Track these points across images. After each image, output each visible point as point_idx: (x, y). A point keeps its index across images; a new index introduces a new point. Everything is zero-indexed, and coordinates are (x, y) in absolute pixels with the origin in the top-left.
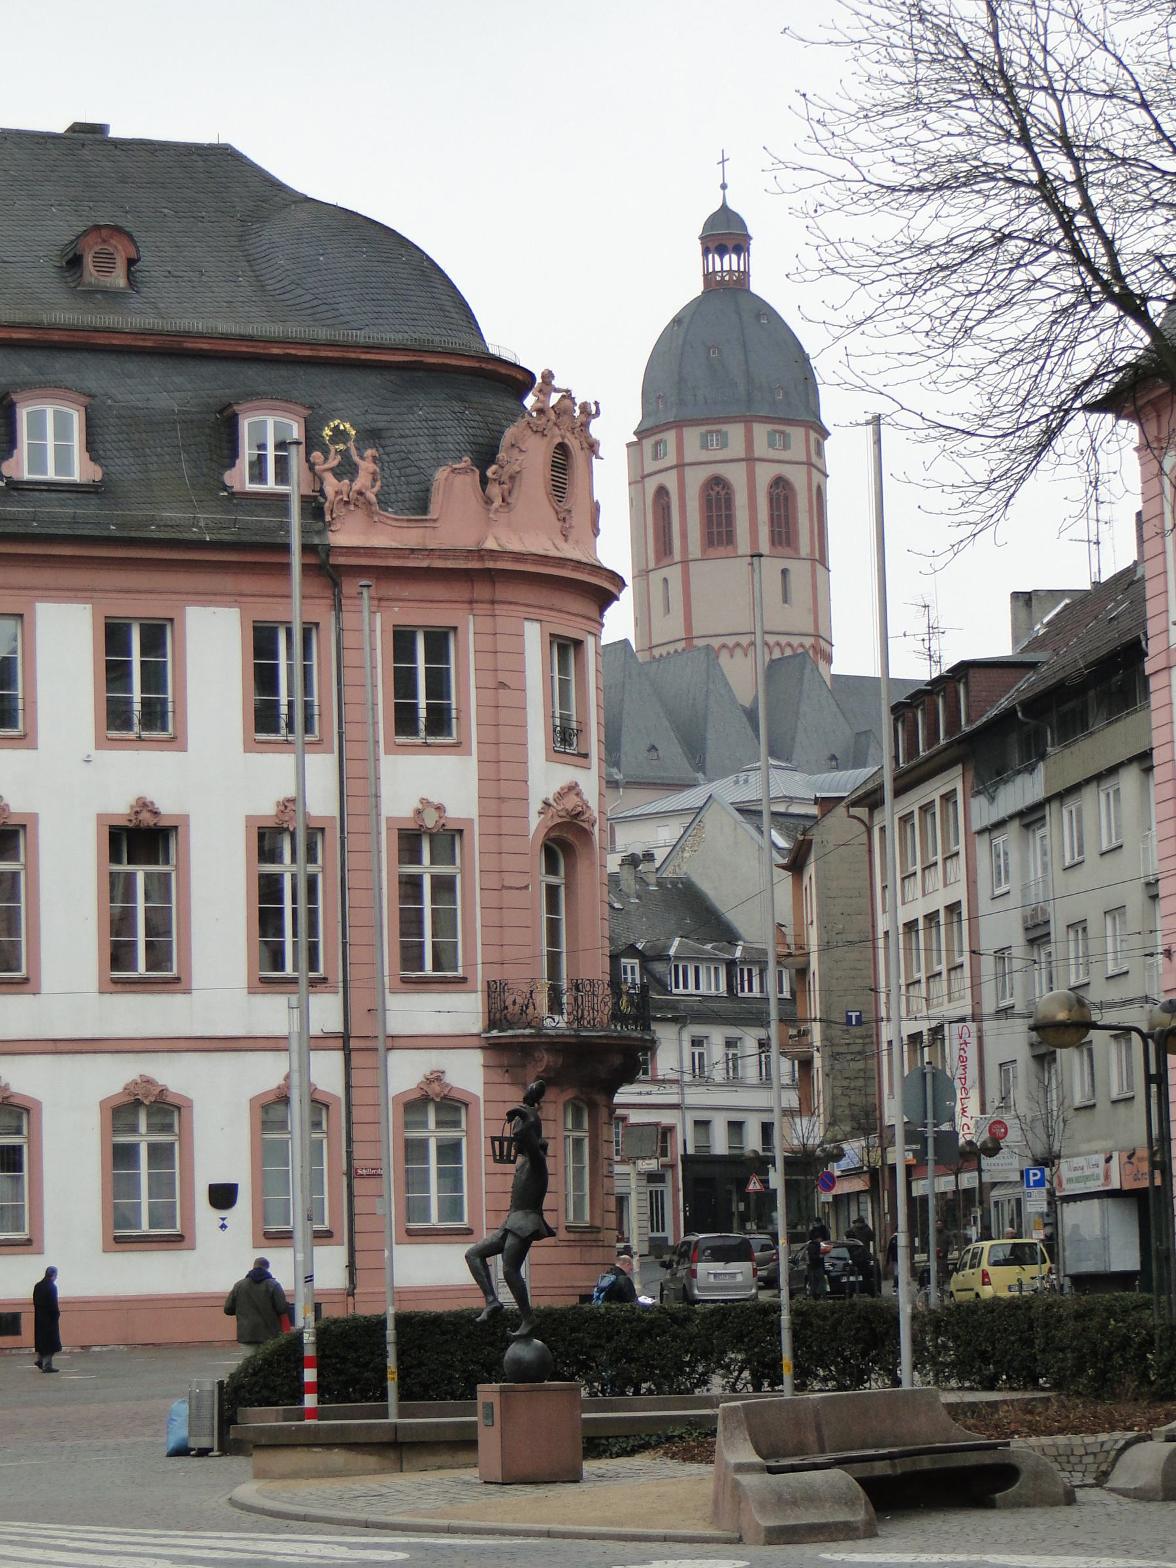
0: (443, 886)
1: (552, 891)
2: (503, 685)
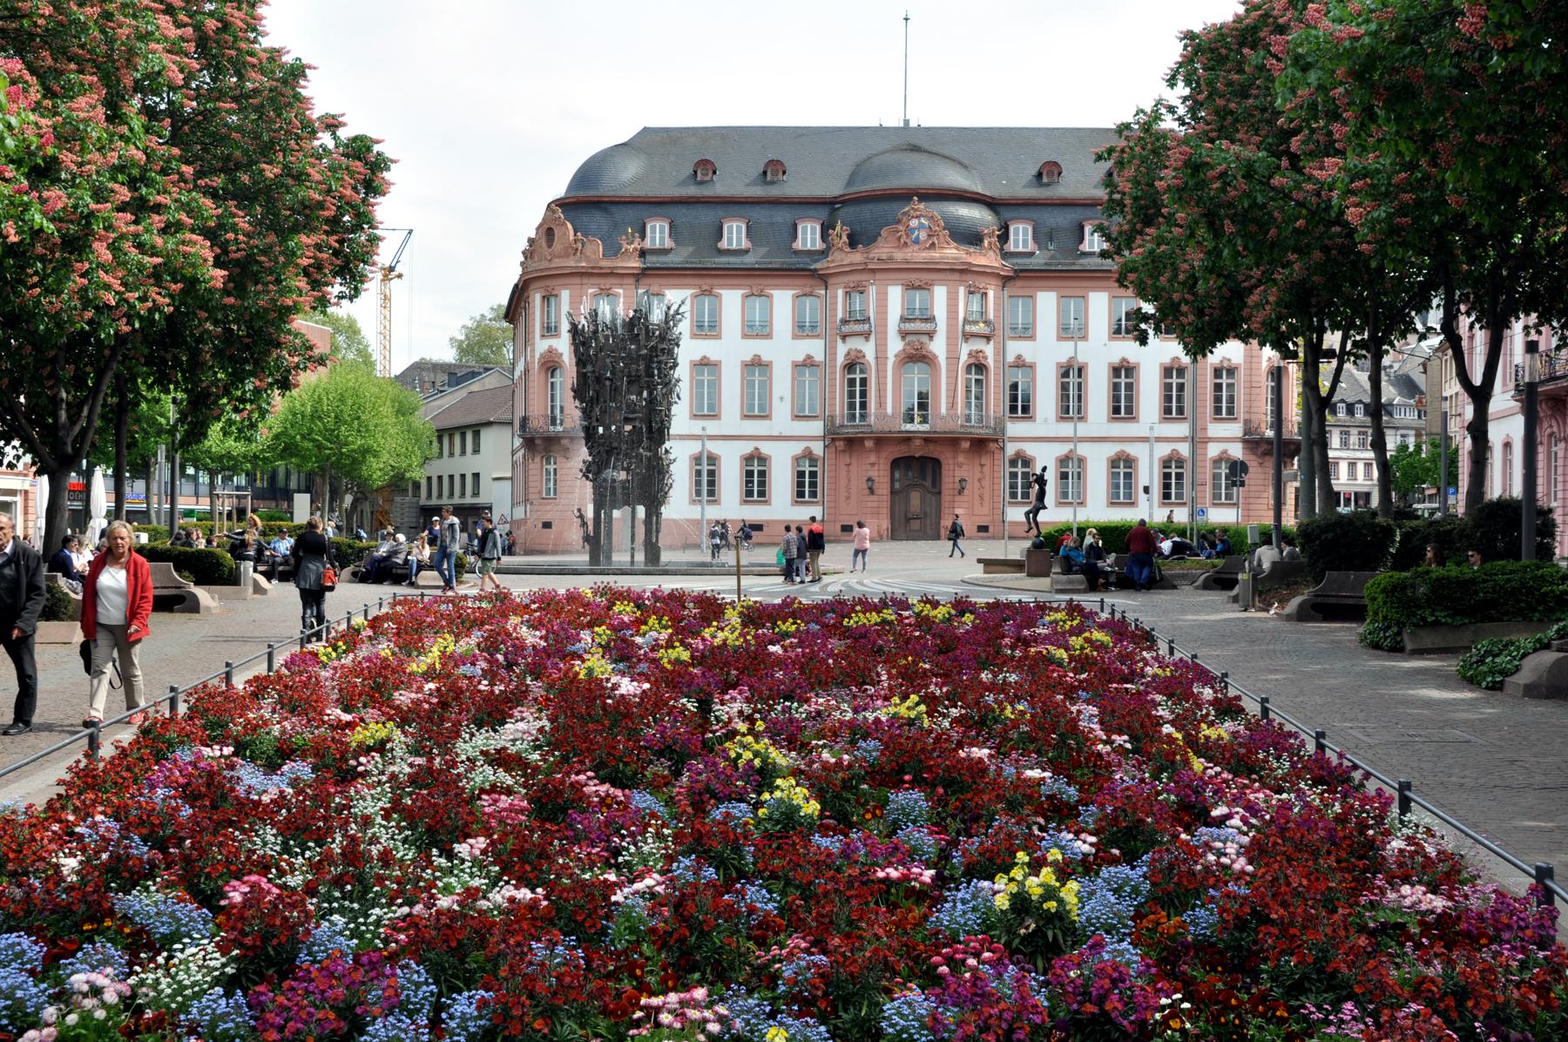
0: (1181, 387)
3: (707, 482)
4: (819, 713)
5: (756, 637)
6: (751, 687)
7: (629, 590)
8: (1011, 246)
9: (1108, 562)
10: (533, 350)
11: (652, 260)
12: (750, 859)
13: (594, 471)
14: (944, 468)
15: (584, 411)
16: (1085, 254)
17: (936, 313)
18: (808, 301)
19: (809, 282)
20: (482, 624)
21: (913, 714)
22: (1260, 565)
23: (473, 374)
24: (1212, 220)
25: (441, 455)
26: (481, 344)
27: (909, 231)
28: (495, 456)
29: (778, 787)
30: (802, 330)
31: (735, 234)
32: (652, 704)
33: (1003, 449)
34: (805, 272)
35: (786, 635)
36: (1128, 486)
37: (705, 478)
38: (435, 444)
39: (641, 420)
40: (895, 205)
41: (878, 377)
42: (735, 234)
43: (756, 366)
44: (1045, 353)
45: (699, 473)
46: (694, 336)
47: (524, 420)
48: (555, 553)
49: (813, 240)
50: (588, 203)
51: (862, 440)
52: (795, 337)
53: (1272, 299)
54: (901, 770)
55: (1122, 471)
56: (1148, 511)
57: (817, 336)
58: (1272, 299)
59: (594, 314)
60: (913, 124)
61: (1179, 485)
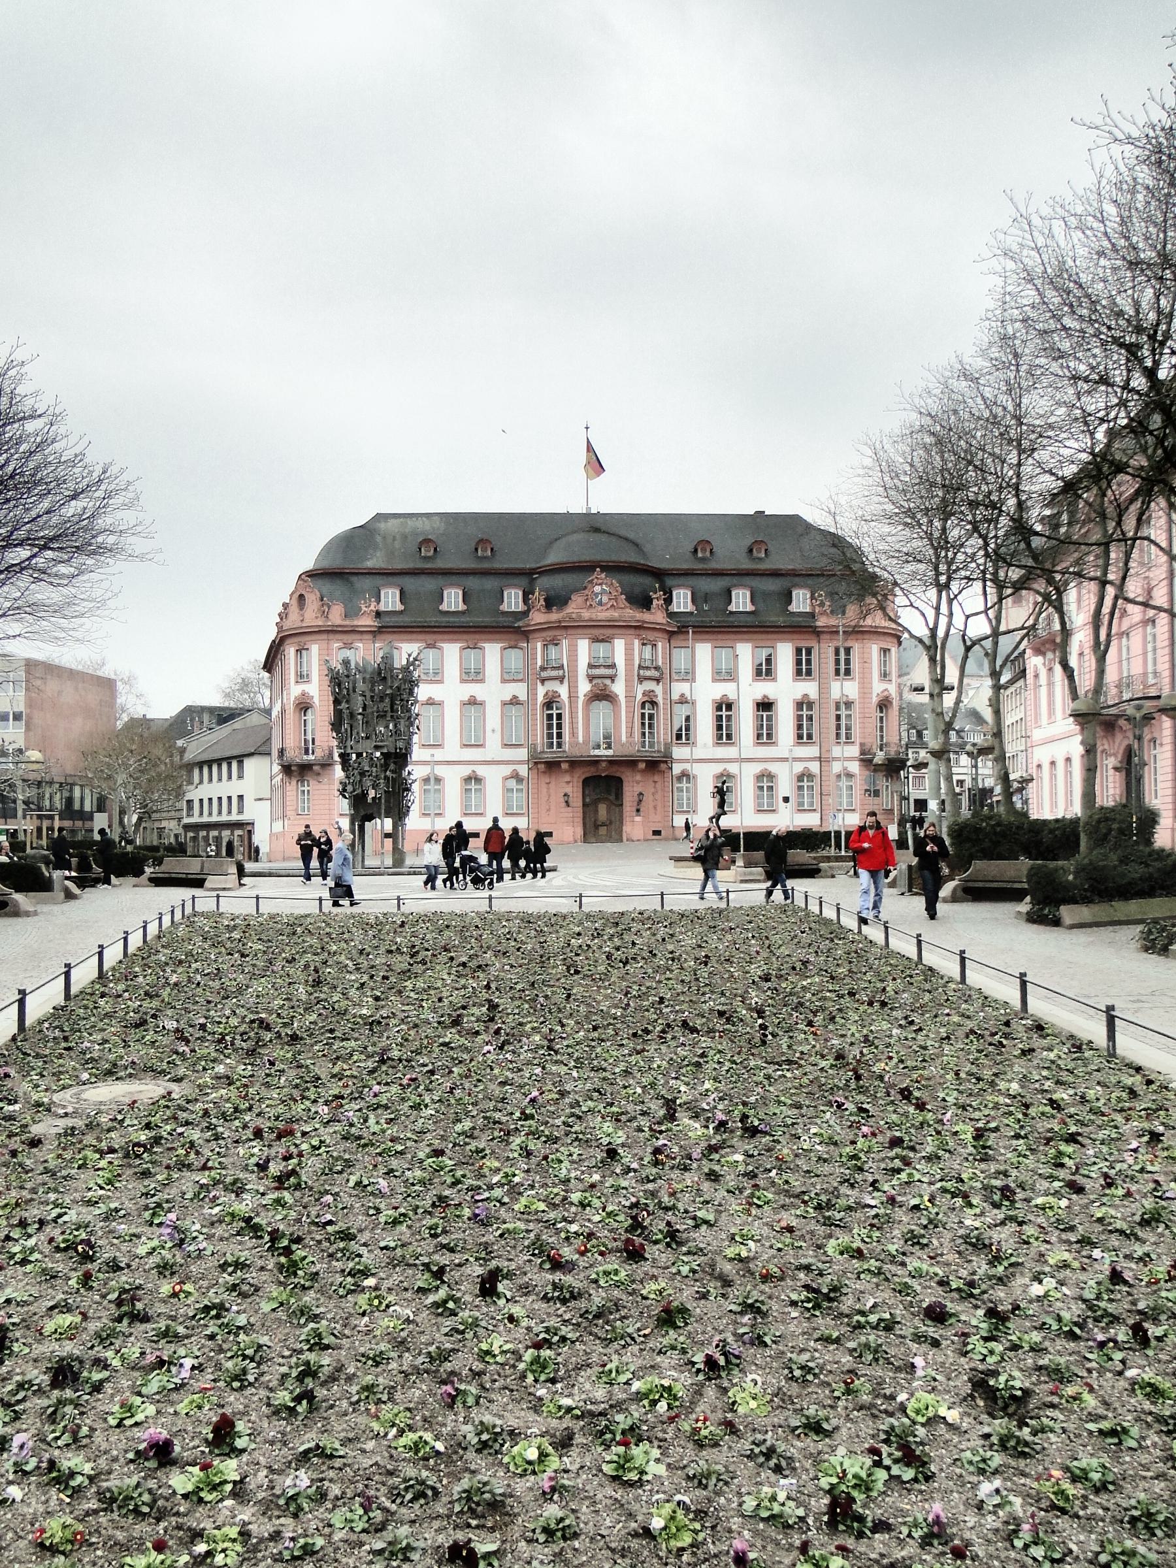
0: (810, 718)
2: (865, 662)
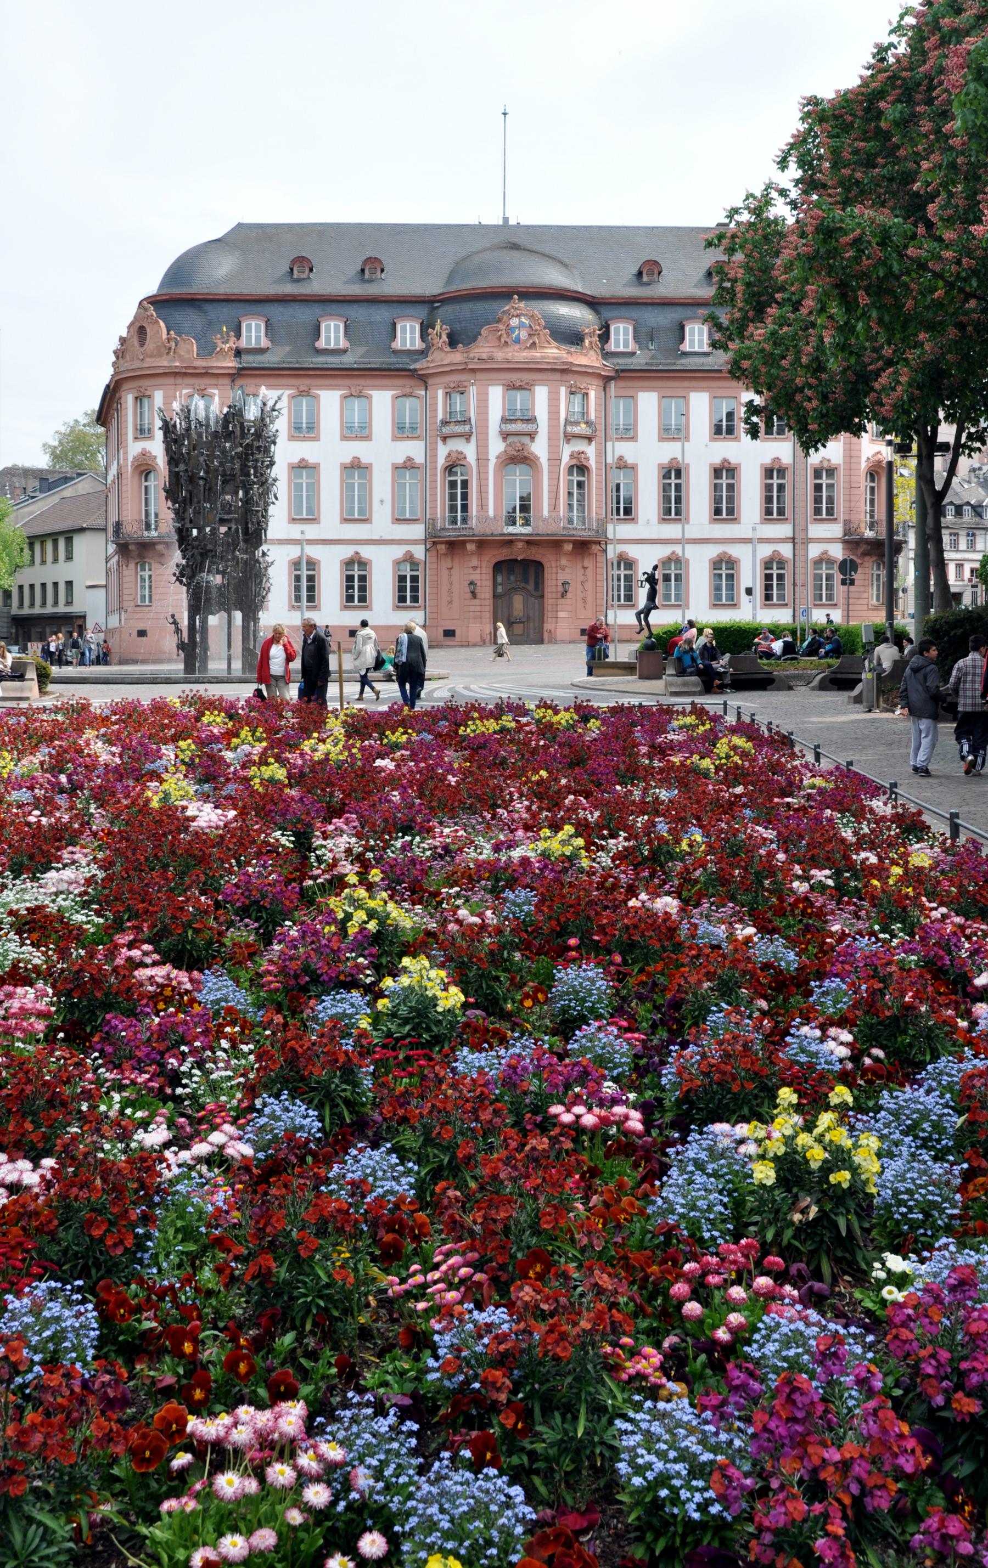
0: (781, 488)
1: (872, 489)
3: (306, 587)
4: (446, 848)
5: (362, 749)
6: (361, 817)
7: (221, 699)
8: (612, 346)
9: (722, 663)
10: (126, 453)
11: (248, 360)
12: (368, 1083)
13: (188, 575)
14: (547, 571)
15: (177, 512)
16: (685, 354)
17: (537, 414)
18: (408, 403)
19: (408, 382)
20: (52, 739)
21: (568, 851)
22: (880, 664)
23: (66, 480)
24: (844, 291)
25: (32, 562)
26: (75, 450)
27: (510, 329)
28: (90, 560)
29: (405, 970)
30: (401, 431)
31: (332, 333)
32: (236, 842)
33: (605, 551)
34: (404, 372)
35: (396, 746)
36: (730, 588)
37: (304, 584)
38: (27, 551)
39: (237, 521)
40: (494, 304)
41: (479, 479)
42: (332, 333)
43: (356, 468)
44: (647, 454)
45: (298, 578)
46: (292, 438)
47: (118, 525)
48: (144, 662)
49: (413, 339)
50: (181, 300)
51: (463, 543)
52: (395, 438)
53: (903, 379)
54: (563, 932)
55: (724, 572)
56: (750, 612)
57: (417, 438)
58: (903, 379)
59: (186, 413)
60: (512, 222)
61: (781, 586)
